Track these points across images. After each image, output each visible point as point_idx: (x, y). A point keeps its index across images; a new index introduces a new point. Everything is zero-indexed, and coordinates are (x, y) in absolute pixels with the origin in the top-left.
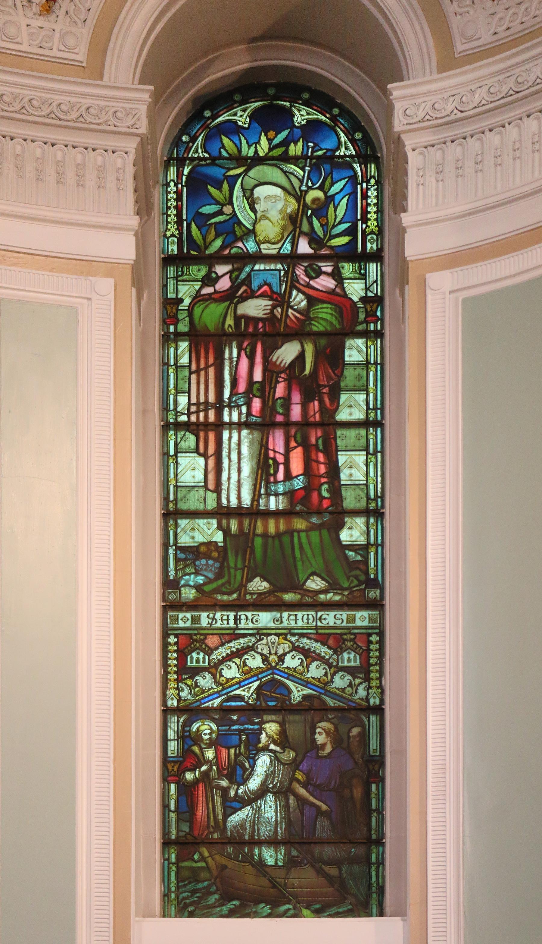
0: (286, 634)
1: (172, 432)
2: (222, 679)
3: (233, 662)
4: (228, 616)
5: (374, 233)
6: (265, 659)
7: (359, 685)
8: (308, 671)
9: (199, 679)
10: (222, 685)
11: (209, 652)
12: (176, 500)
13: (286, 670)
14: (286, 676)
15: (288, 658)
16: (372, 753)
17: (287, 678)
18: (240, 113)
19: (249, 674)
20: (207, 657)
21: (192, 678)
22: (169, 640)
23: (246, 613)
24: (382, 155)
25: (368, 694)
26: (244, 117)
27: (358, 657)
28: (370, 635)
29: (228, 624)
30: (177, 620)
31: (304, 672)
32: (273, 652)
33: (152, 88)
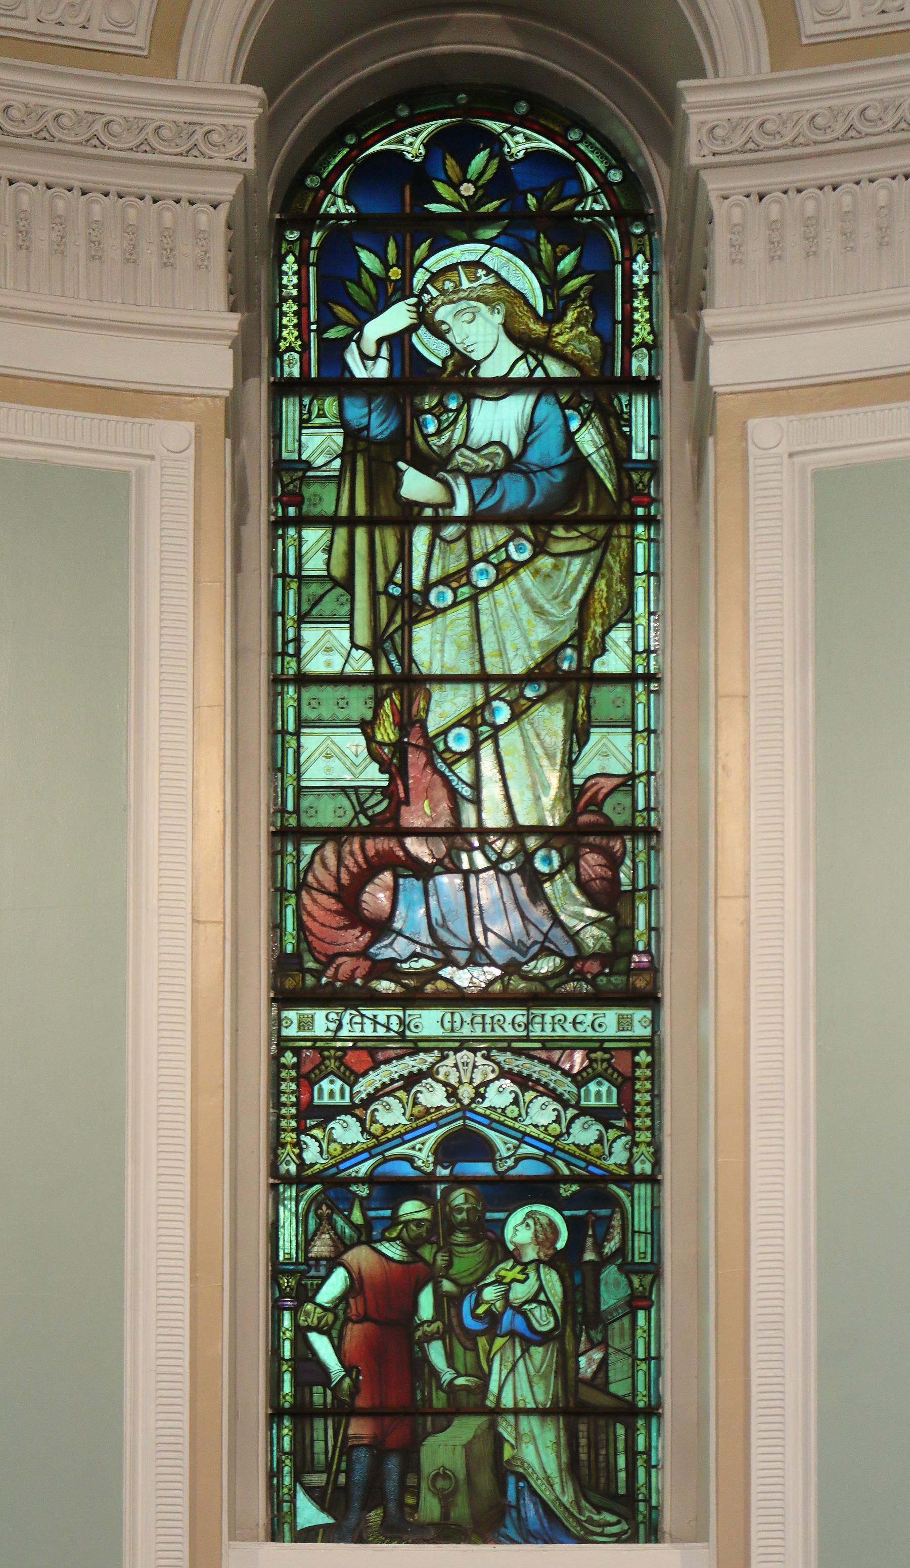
5: (293, 350)
6: (452, 1094)
7: (614, 1141)
8: (527, 1113)
11: (351, 1077)
12: (297, 810)
14: (486, 1122)
16: (637, 1260)
18: (409, 140)
19: (424, 1118)
20: (347, 1088)
21: (322, 1125)
24: (658, 212)
25: (632, 1155)
26: (520, 148)
27: (614, 1090)
28: (635, 1051)
29: (362, 1030)
30: (631, 1024)
31: (520, 1115)
32: (465, 1079)
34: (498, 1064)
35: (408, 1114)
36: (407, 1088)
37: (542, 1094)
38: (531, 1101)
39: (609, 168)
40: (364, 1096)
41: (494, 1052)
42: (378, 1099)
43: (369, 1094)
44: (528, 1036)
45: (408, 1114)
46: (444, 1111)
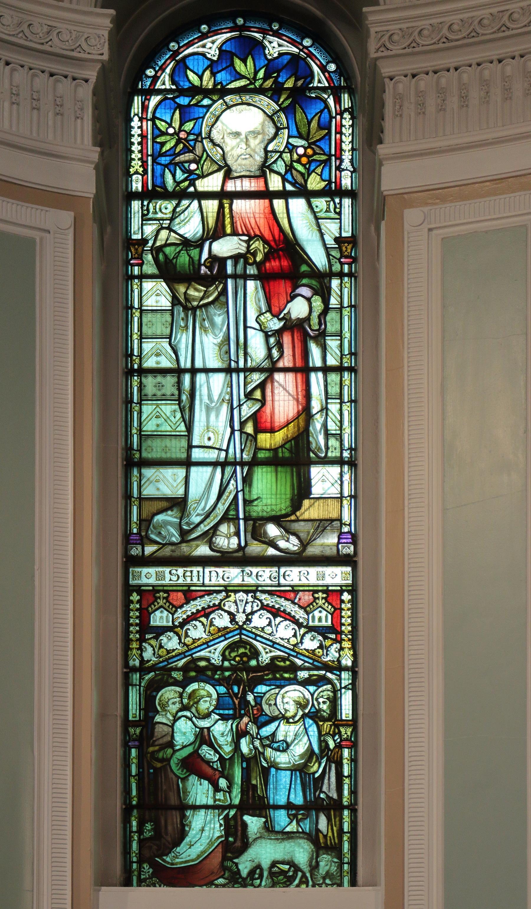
0: (254, 592)
1: (136, 378)
2: (188, 639)
3: (200, 621)
4: (191, 572)
6: (233, 619)
8: (277, 631)
9: (164, 639)
10: (188, 646)
11: (173, 608)
13: (254, 630)
15: (255, 617)
17: (255, 639)
20: (170, 615)
21: (156, 638)
22: (131, 598)
23: (218, 569)
27: (330, 616)
29: (192, 580)
30: (140, 576)
31: (272, 632)
32: (241, 610)
33: (112, 12)
34: (261, 601)
35: (207, 631)
36: (207, 616)
37: (286, 619)
38: (279, 624)
39: (328, 63)
40: (181, 620)
41: (258, 594)
42: (189, 623)
43: (184, 619)
44: (279, 583)
45: (207, 631)
46: (228, 630)
